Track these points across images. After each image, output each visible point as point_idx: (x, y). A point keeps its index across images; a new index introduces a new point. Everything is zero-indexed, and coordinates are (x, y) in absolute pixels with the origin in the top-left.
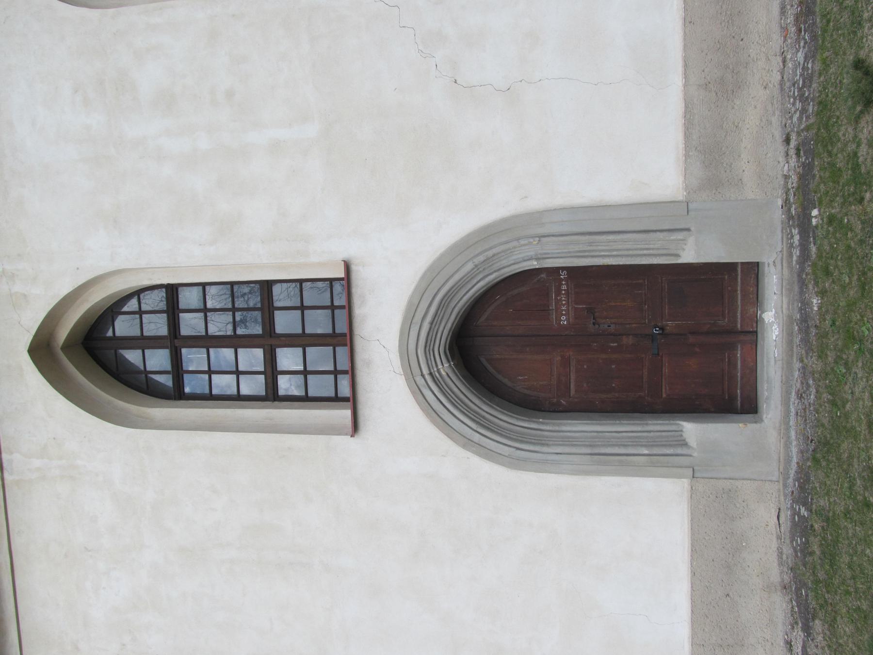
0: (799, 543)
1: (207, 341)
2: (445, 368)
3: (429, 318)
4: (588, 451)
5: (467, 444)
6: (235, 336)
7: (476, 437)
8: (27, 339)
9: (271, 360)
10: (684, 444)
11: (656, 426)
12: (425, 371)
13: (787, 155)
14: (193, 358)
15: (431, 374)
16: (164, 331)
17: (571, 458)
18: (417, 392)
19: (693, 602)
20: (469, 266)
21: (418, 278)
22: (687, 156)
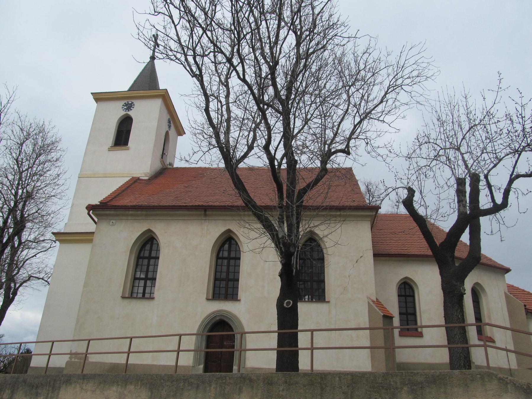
0: (284, 250)
1: (228, 266)
2: (218, 318)
3: (227, 316)
4: (199, 346)
5: (203, 322)
6: (229, 266)
7: (204, 324)
8: (232, 229)
9: (223, 280)
10: (199, 365)
11: (203, 360)
12: (217, 315)
13: (65, 173)
14: (225, 262)
15: (217, 316)
16: (224, 282)
17: (198, 343)
18: (213, 313)
19: (168, 365)
20: (237, 325)
21: (235, 314)
22: (253, 368)
